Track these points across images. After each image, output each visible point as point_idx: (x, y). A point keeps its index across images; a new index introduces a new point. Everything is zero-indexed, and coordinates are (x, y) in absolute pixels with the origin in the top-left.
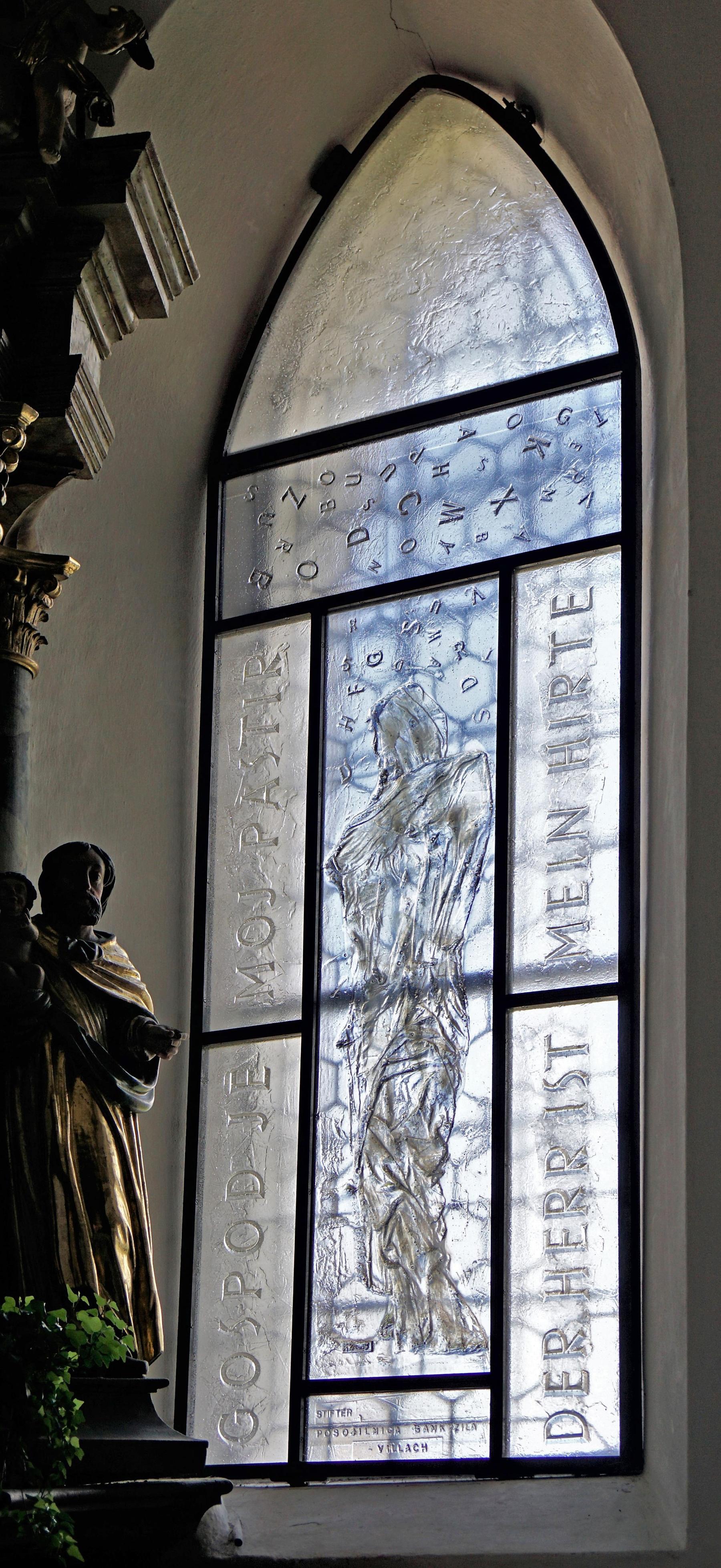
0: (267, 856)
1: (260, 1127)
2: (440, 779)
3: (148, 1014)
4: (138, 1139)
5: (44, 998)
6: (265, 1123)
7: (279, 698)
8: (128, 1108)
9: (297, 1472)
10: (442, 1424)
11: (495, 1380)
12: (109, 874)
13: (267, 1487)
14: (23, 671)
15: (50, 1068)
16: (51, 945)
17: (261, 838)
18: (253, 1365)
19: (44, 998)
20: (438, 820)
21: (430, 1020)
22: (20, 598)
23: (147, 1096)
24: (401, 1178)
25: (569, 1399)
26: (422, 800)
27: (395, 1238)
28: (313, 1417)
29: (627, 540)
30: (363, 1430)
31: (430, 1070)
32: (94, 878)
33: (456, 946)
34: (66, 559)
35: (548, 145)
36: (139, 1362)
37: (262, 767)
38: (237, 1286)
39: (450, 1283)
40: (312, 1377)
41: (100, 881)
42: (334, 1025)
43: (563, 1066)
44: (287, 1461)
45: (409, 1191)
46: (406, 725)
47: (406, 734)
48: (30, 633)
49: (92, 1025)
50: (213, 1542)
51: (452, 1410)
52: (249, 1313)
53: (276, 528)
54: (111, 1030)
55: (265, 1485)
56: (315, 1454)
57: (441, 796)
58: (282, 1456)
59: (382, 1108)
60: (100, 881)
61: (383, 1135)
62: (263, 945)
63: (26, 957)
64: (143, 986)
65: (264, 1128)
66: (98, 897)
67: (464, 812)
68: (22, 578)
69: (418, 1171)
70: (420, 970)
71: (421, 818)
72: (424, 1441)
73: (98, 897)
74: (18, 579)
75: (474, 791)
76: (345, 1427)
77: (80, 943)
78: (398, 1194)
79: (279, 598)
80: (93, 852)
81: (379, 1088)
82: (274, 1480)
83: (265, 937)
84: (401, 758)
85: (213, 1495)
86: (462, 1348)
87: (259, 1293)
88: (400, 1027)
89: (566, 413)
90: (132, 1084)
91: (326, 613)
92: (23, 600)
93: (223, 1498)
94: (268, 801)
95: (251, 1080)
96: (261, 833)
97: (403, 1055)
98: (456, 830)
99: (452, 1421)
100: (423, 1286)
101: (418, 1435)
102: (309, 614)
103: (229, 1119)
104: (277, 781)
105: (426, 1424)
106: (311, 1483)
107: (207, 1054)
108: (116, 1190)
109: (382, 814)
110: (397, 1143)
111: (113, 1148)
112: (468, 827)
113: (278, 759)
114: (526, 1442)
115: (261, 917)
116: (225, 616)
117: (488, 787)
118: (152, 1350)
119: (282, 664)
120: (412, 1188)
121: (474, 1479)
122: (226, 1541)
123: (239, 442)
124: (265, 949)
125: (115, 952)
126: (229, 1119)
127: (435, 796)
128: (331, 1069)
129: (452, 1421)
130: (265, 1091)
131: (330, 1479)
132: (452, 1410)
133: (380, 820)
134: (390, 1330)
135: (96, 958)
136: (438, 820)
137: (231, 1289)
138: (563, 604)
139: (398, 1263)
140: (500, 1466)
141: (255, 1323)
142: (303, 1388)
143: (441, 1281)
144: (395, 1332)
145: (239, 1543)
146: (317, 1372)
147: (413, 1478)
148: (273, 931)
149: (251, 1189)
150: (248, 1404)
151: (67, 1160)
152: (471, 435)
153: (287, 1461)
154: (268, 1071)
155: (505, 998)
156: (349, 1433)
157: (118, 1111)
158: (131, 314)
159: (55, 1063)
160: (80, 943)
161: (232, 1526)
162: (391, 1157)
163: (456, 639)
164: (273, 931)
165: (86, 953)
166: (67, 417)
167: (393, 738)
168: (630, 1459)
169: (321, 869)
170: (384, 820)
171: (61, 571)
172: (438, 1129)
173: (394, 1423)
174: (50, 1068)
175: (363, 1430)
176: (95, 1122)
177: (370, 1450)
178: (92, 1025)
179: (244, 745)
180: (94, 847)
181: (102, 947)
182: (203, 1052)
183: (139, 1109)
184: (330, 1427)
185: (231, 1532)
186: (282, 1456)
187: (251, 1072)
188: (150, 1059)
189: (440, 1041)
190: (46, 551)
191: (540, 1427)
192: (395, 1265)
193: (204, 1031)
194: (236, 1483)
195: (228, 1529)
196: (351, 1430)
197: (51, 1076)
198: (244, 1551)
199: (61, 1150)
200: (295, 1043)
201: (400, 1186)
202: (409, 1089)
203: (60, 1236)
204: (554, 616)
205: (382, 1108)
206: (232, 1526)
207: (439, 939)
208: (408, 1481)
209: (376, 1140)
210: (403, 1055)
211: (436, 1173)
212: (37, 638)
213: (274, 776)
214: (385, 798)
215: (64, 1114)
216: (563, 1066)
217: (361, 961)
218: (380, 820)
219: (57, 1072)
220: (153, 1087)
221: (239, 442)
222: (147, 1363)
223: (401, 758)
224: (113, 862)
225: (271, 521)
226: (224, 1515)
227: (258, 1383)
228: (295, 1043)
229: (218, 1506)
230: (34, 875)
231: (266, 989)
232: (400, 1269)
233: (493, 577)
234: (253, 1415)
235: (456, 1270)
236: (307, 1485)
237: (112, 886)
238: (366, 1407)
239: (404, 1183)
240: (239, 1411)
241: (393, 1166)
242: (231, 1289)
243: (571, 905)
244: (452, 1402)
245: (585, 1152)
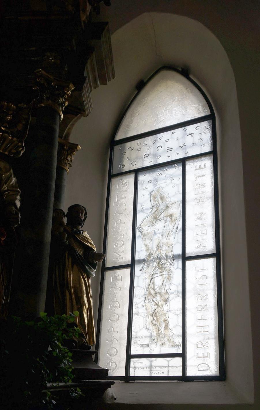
0: (122, 226)
1: (119, 290)
2: (167, 207)
3: (94, 250)
4: (90, 284)
5: (66, 241)
6: (120, 289)
7: (126, 191)
8: (89, 275)
9: (127, 379)
10: (165, 367)
11: (183, 355)
12: (86, 214)
13: (119, 383)
14: (65, 171)
15: (67, 260)
16: (69, 229)
17: (121, 222)
18: (116, 350)
19: (66, 241)
20: (167, 216)
21: (164, 264)
22: (66, 152)
23: (94, 273)
24: (157, 303)
25: (204, 362)
26: (162, 212)
27: (155, 318)
28: (132, 365)
29: (213, 153)
30: (146, 368)
31: (164, 276)
32: (82, 213)
33: (170, 246)
34: (78, 145)
35: (191, 77)
36: (89, 346)
37: (122, 206)
38: (112, 330)
39: (170, 329)
40: (131, 354)
41: (83, 215)
42: (137, 268)
43: (200, 274)
44: (124, 376)
45: (159, 306)
46: (158, 197)
47: (158, 197)
48: (67, 162)
49: (80, 252)
50: (107, 398)
51: (168, 363)
52: (115, 337)
53: (126, 155)
54: (84, 254)
55: (118, 382)
56: (132, 374)
57: (167, 211)
58: (123, 374)
59: (151, 286)
60: (83, 215)
61: (151, 293)
62: (121, 246)
63: (62, 231)
64: (93, 244)
65: (120, 291)
66: (83, 219)
67: (173, 215)
68: (66, 148)
69: (161, 301)
70: (162, 251)
71: (162, 216)
72: (163, 371)
73: (83, 219)
74: (65, 148)
75: (177, 211)
76: (141, 367)
77: (77, 230)
78: (156, 306)
79: (126, 169)
80: (82, 207)
81: (151, 280)
82: (121, 381)
83: (121, 245)
84: (157, 203)
85: (109, 385)
86: (174, 346)
87: (118, 332)
88: (156, 266)
89: (198, 127)
90: (90, 268)
91: (138, 172)
92: (66, 153)
93: (112, 386)
94: (123, 214)
95: (117, 279)
96: (121, 221)
97: (157, 272)
98: (171, 218)
99: (169, 366)
100: (162, 330)
101: (161, 369)
102: (134, 172)
103: (111, 288)
104: (125, 209)
105: (163, 367)
106: (131, 382)
107: (105, 273)
108: (84, 296)
109: (152, 215)
110: (156, 294)
111: (83, 285)
112: (174, 218)
113: (126, 204)
114: (191, 372)
115: (121, 240)
116: (113, 174)
117: (179, 208)
118: (92, 343)
119: (127, 184)
120: (160, 305)
121: (177, 381)
122: (110, 398)
123: (119, 137)
124: (121, 248)
125: (86, 234)
126: (111, 288)
127: (166, 211)
128: (137, 278)
129: (169, 366)
130: (121, 281)
131: (136, 381)
132: (168, 363)
133: (152, 217)
134: (153, 342)
135: (81, 234)
136: (167, 216)
137: (110, 331)
138: (198, 167)
139: (156, 324)
140: (184, 378)
141: (116, 340)
142: (129, 357)
143: (167, 329)
144: (155, 342)
145: (115, 399)
146: (133, 353)
147: (151, 381)
148: (123, 243)
149: (116, 306)
150: (114, 361)
151: (71, 286)
152: (174, 133)
153: (124, 376)
154: (121, 277)
155: (184, 258)
156: (140, 369)
157: (85, 275)
158: (99, 83)
159: (68, 260)
160: (77, 230)
161: (112, 394)
162: (154, 297)
163: (168, 182)
164: (123, 243)
165: (79, 233)
166: (82, 92)
167: (155, 198)
168: (222, 376)
169: (136, 229)
170: (152, 217)
171: (76, 148)
172: (167, 290)
173: (151, 367)
174: (67, 260)
175: (146, 368)
176: (80, 277)
177: (145, 373)
178: (80, 252)
179: (117, 201)
180: (82, 206)
181: (83, 232)
182: (105, 272)
183: (91, 276)
184: (135, 367)
185: (112, 395)
186: (123, 374)
187: (117, 277)
188: (95, 262)
189: (167, 268)
190: (73, 142)
191: (196, 368)
192: (155, 325)
193: (105, 267)
194: (116, 382)
195: (111, 395)
196: (142, 368)
197: (67, 262)
198: (116, 401)
199: (69, 283)
200: (128, 270)
201: (157, 305)
202: (158, 281)
203: (67, 308)
204: (196, 170)
205: (151, 286)
206: (112, 394)
207: (167, 244)
208: (159, 382)
209: (150, 294)
210: (157, 272)
211: (166, 301)
212: (69, 164)
213: (124, 208)
214: (152, 212)
215: (70, 273)
216: (200, 274)
217: (146, 250)
218: (152, 217)
219: (69, 263)
220: (95, 270)
221: (119, 137)
222: (91, 346)
223: (157, 203)
224: (87, 211)
225: (125, 153)
226: (111, 391)
227: (117, 355)
228: (128, 270)
229: (109, 389)
230: (66, 211)
231: (121, 257)
232: (156, 326)
233: (181, 162)
234: (115, 363)
235: (171, 326)
236: (130, 382)
237: (86, 217)
238: (145, 362)
239: (157, 303)
240: (112, 362)
241: (154, 300)
242: (110, 331)
243: (202, 236)
244: (168, 361)
245: (207, 296)
